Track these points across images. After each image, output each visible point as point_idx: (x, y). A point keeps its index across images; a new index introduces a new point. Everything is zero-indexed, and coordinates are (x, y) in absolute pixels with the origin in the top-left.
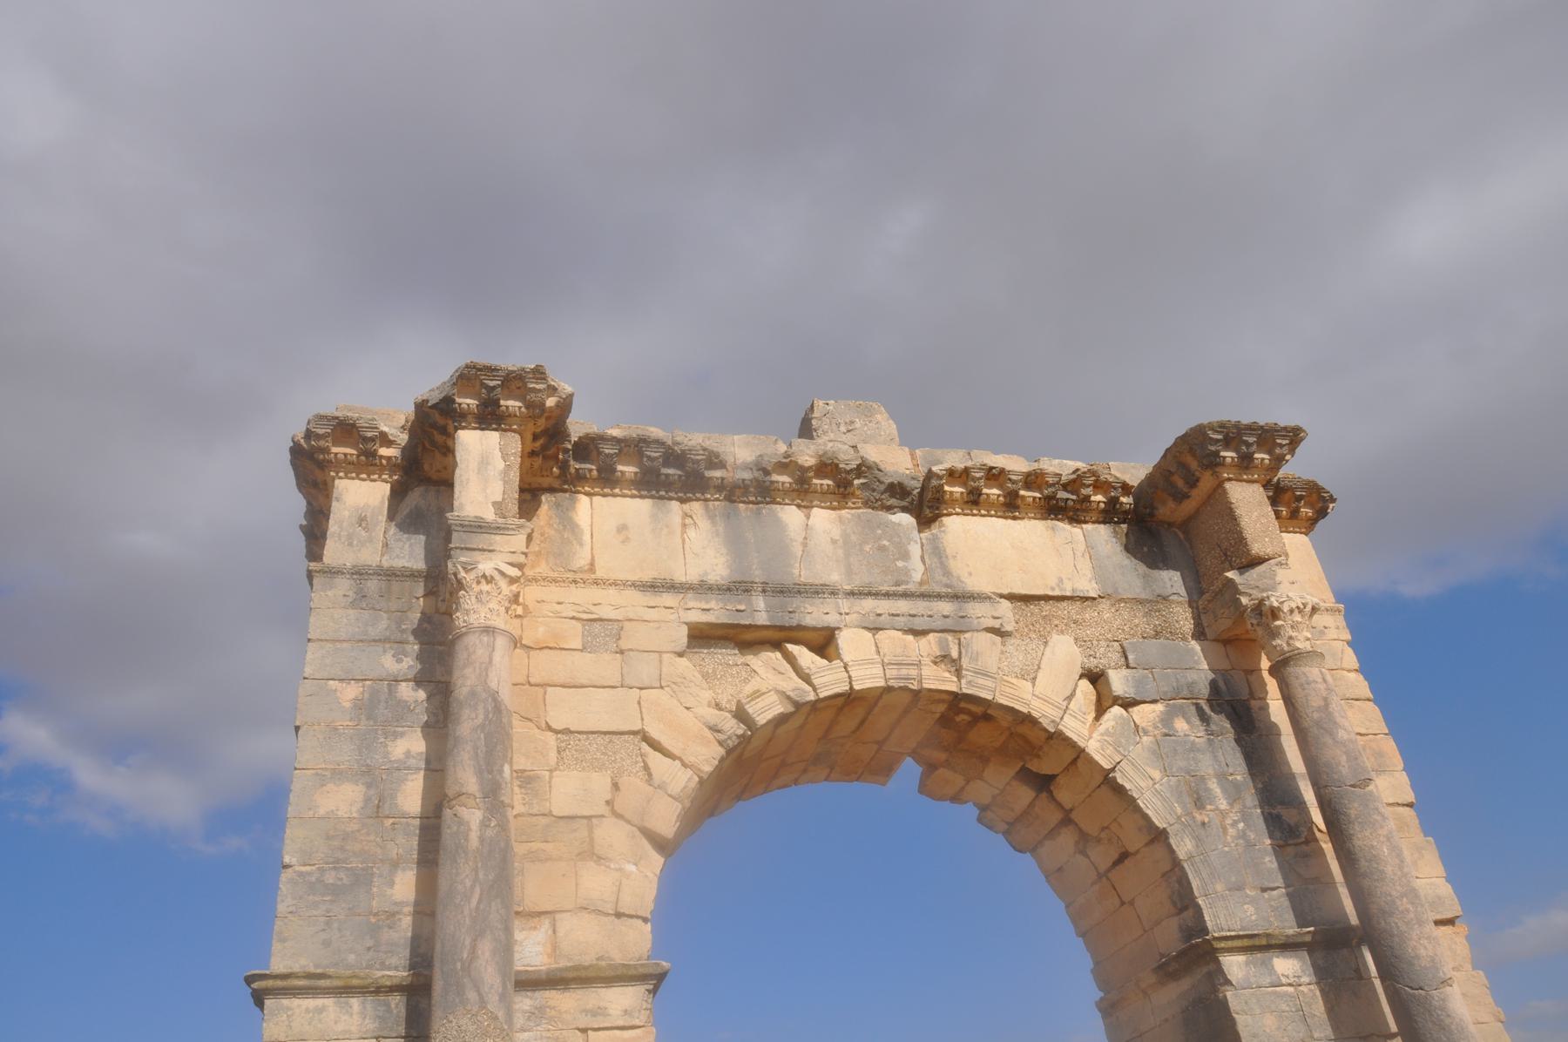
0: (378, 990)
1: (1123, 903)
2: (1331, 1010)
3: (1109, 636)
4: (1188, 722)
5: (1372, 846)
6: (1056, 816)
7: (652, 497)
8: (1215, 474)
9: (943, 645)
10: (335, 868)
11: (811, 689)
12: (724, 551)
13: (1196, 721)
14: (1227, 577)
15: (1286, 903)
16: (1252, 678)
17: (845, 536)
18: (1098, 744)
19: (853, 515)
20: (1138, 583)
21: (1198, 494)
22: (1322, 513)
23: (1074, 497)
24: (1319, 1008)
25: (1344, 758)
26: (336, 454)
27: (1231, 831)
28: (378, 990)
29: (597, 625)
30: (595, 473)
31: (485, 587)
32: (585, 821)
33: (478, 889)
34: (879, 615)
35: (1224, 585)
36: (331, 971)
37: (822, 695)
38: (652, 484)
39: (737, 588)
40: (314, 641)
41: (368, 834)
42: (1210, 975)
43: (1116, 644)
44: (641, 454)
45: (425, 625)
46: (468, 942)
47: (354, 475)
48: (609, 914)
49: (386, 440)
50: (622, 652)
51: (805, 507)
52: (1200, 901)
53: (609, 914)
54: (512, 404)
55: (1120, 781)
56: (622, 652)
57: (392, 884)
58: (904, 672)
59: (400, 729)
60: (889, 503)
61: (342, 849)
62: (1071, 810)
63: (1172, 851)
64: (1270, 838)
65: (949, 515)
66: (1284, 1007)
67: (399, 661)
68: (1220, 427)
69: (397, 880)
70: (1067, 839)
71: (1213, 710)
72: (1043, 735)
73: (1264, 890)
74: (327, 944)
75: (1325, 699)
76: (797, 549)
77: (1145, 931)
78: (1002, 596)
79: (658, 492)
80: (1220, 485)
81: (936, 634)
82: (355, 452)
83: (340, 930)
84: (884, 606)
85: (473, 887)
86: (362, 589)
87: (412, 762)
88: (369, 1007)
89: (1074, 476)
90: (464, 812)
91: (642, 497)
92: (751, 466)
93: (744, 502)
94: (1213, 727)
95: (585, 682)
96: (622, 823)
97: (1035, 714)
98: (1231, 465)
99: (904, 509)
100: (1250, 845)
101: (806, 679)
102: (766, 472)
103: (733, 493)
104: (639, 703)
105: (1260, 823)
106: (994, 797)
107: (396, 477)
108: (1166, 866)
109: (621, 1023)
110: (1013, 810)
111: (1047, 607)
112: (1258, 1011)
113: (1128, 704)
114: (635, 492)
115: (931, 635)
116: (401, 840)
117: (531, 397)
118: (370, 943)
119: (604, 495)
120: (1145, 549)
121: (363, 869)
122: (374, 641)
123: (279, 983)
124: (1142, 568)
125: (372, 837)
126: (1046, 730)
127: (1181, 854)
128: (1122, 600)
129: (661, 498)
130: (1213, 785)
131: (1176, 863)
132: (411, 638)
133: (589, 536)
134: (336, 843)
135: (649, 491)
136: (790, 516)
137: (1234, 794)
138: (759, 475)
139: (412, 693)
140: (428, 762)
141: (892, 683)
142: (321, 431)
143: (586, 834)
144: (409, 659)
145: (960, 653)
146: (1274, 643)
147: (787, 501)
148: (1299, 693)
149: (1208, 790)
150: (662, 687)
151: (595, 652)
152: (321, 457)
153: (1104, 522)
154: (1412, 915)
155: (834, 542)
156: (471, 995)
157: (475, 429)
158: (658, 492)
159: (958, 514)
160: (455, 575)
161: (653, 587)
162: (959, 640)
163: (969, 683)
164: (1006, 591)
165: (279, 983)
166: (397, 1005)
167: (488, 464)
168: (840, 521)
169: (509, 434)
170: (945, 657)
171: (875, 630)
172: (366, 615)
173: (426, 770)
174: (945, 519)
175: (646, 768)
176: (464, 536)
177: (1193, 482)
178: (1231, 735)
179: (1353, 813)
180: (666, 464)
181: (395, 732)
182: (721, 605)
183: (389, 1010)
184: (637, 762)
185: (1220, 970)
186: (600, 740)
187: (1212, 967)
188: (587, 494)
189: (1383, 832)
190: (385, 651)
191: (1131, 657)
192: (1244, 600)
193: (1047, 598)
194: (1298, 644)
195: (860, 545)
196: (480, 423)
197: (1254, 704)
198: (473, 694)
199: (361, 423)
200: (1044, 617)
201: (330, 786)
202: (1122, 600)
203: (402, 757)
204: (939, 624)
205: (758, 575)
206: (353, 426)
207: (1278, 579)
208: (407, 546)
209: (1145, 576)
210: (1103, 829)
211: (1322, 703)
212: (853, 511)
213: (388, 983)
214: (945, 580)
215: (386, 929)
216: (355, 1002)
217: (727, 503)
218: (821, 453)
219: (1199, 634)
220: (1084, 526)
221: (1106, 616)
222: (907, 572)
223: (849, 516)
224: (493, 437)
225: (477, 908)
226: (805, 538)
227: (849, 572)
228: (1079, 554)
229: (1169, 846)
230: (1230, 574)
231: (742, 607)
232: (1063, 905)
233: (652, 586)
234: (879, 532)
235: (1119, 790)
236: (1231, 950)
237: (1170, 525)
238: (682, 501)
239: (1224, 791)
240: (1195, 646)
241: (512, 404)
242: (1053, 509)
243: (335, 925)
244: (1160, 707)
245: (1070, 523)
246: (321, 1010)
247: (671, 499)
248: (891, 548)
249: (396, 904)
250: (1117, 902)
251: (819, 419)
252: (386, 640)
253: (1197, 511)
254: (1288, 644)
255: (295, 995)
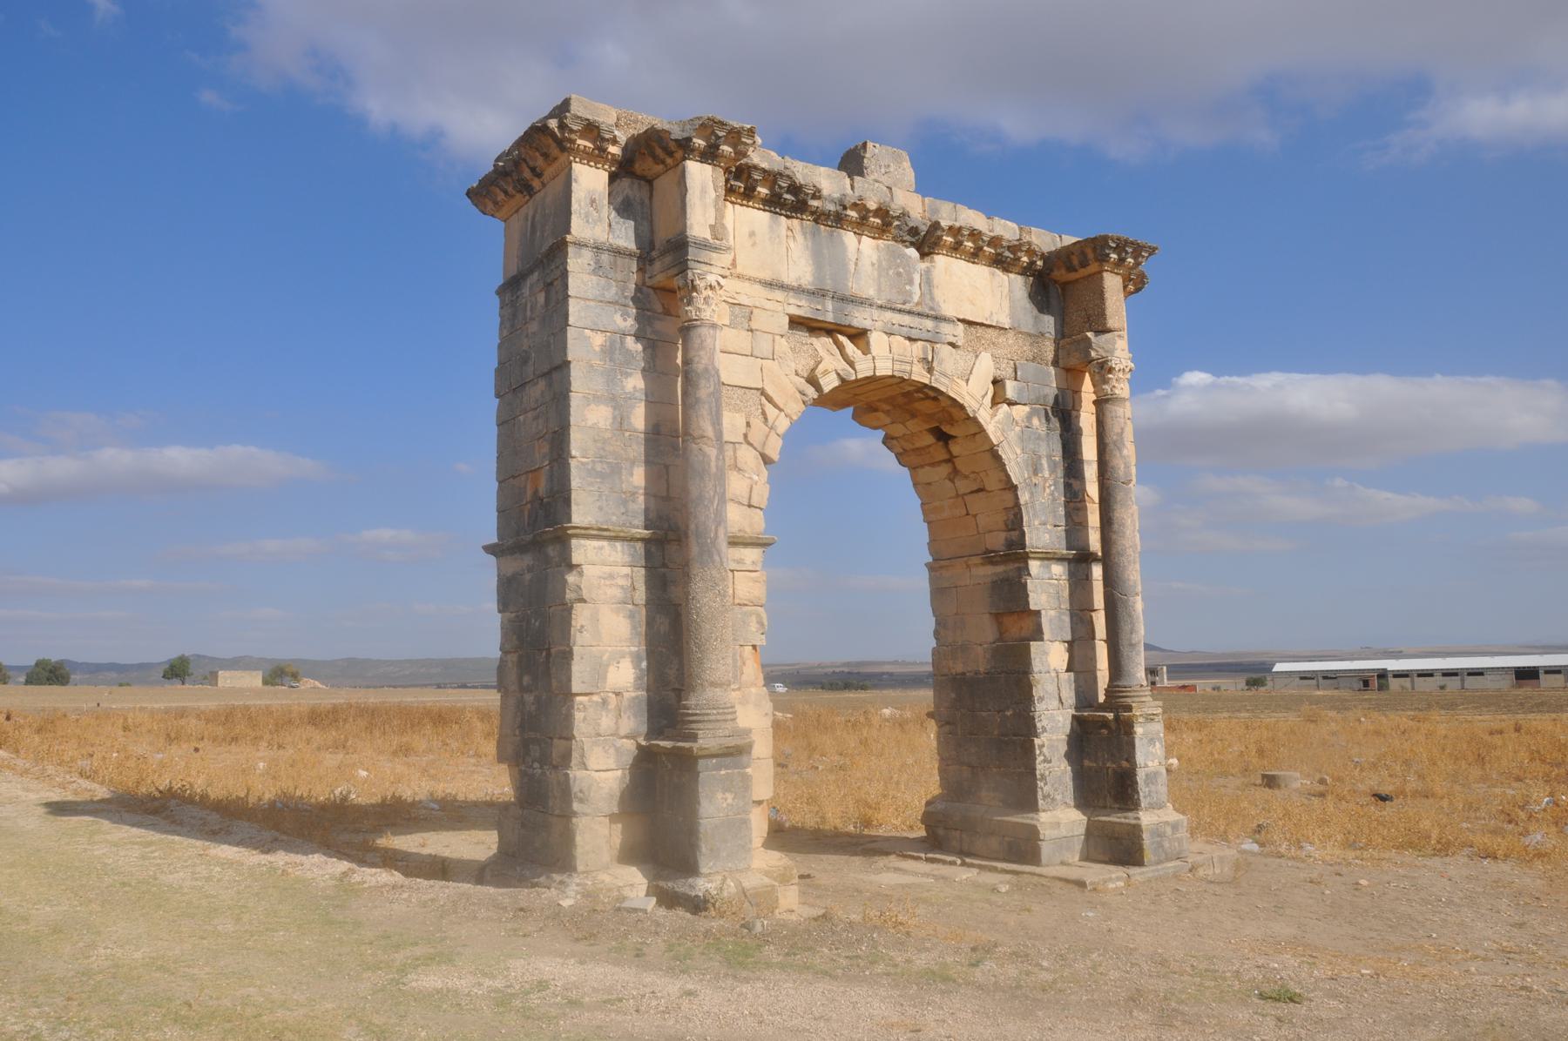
0: (632, 539)
1: (968, 514)
2: (1071, 595)
3: (1009, 356)
4: (1040, 421)
5: (1123, 518)
6: (944, 456)
7: (771, 211)
8: (1101, 266)
9: (925, 350)
10: (601, 462)
11: (853, 372)
12: (811, 262)
13: (1044, 420)
14: (1087, 336)
15: (1063, 534)
16: (1076, 396)
17: (879, 261)
18: (994, 429)
19: (885, 245)
20: (1031, 321)
21: (1083, 272)
22: (1137, 290)
23: (1012, 256)
24: (1066, 593)
25: (1122, 466)
26: (579, 145)
27: (1048, 491)
28: (632, 539)
29: (737, 308)
30: (742, 190)
31: (709, 292)
32: (732, 445)
33: (717, 498)
34: (894, 324)
35: (1082, 339)
36: (611, 527)
37: (859, 377)
38: (774, 203)
39: (818, 293)
40: (967, 511)
41: (617, 441)
42: (1019, 569)
43: (1012, 362)
44: (775, 182)
45: (639, 295)
46: (713, 527)
47: (586, 162)
48: (744, 505)
49: (614, 141)
50: (752, 331)
51: (859, 234)
52: (1025, 529)
53: (744, 505)
54: (726, 149)
55: (1000, 453)
56: (752, 331)
57: (632, 475)
58: (903, 367)
59: (629, 370)
60: (905, 239)
61: (603, 449)
62: (956, 457)
63: (1017, 498)
64: (1065, 497)
65: (938, 254)
66: (1051, 591)
67: (625, 320)
68: (1118, 239)
69: (635, 473)
70: (945, 470)
71: (1053, 414)
72: (964, 416)
73: (1055, 526)
74: (601, 508)
75: (1122, 429)
76: (852, 267)
77: (979, 533)
78: (959, 320)
79: (775, 208)
80: (1100, 272)
81: (922, 343)
82: (592, 146)
83: (607, 501)
84: (898, 318)
85: (714, 496)
86: (599, 260)
87: (637, 394)
88: (625, 547)
89: (1017, 243)
90: (707, 449)
91: (764, 210)
92: (835, 201)
93: (824, 225)
94: (1051, 426)
95: (731, 350)
96: (751, 448)
97: (966, 405)
98: (1112, 262)
99: (912, 244)
100: (1054, 500)
101: (851, 364)
102: (845, 208)
103: (819, 217)
104: (761, 369)
105: (1061, 487)
106: (904, 435)
107: (613, 169)
108: (1011, 504)
109: (751, 569)
110: (913, 444)
111: (980, 330)
112: (1040, 590)
113: (1011, 403)
114: (761, 206)
115: (919, 342)
116: (635, 447)
117: (741, 147)
118: (623, 510)
119: (742, 205)
120: (1039, 298)
121: (616, 464)
122: (609, 302)
123: (583, 532)
124: (1035, 311)
125: (618, 443)
126: (968, 415)
127: (1022, 501)
128: (1020, 333)
129: (776, 213)
130: (1044, 462)
131: (1017, 505)
132: (631, 303)
133: (732, 237)
134: (599, 445)
135: (770, 207)
136: (849, 238)
137: (1053, 471)
138: (839, 208)
139: (634, 345)
140: (646, 395)
141: (896, 374)
142: (575, 128)
143: (732, 454)
144: (630, 319)
145: (933, 357)
146: (1104, 387)
147: (850, 229)
148: (1108, 421)
149: (1041, 464)
150: (773, 359)
151: (736, 328)
152: (569, 145)
153: (1021, 275)
154: (1132, 558)
155: (873, 264)
156: (716, 558)
157: (697, 161)
158: (775, 208)
159: (943, 254)
160: (692, 281)
161: (770, 285)
162: (933, 348)
163: (936, 380)
164: (961, 317)
165: (583, 532)
166: (640, 548)
167: (706, 192)
168: (878, 249)
169: (718, 168)
170: (924, 359)
171: (890, 334)
172: (603, 281)
173: (646, 401)
174: (936, 257)
175: (764, 413)
176: (696, 251)
177: (1084, 264)
178: (1058, 432)
179: (1119, 498)
180: (788, 192)
181: (627, 372)
182: (808, 304)
183: (636, 551)
184: (758, 409)
185: (1027, 568)
186: (742, 391)
187: (1022, 565)
188: (732, 203)
189: (1130, 511)
190: (616, 311)
191: (1019, 373)
192: (1093, 354)
193: (982, 325)
194: (1117, 392)
195: (887, 270)
196: (701, 158)
197: (1074, 413)
198: (706, 370)
199: (603, 127)
200: (977, 337)
201: (593, 406)
202: (1020, 333)
203: (632, 390)
204: (925, 335)
205: (829, 285)
206: (598, 127)
207: (1116, 346)
208: (623, 229)
209: (1036, 317)
210: (974, 472)
211: (1120, 431)
212: (886, 242)
213: (639, 536)
214: (931, 304)
215: (630, 502)
216: (618, 545)
217: (813, 223)
218: (882, 201)
219: (1055, 363)
220: (1010, 275)
221: (1010, 342)
222: (910, 294)
223: (882, 246)
224: (708, 168)
225: (717, 509)
226: (857, 259)
227: (879, 290)
228: (1004, 295)
229: (1017, 495)
230: (1090, 334)
231: (819, 307)
232: (920, 502)
233: (771, 284)
234: (899, 261)
235: (997, 458)
236: (1034, 558)
237: (1056, 282)
238: (788, 217)
239: (1049, 466)
240: (1052, 370)
241: (726, 149)
242: (999, 262)
243: (604, 498)
244: (1027, 409)
245: (1003, 271)
246: (601, 548)
247: (781, 215)
248: (904, 275)
249: (635, 487)
250: (965, 512)
251: (869, 159)
252: (616, 303)
253: (1077, 281)
254: (1112, 390)
255: (588, 538)
